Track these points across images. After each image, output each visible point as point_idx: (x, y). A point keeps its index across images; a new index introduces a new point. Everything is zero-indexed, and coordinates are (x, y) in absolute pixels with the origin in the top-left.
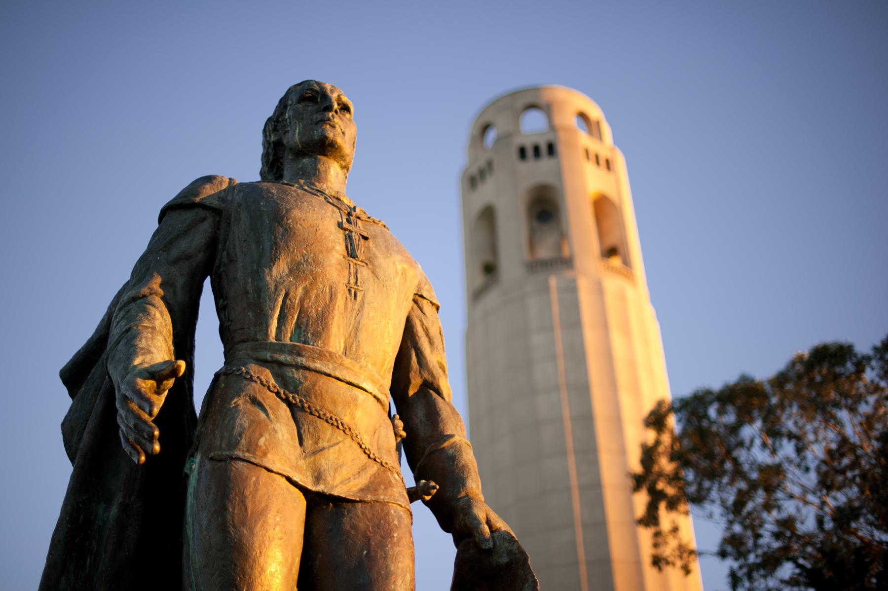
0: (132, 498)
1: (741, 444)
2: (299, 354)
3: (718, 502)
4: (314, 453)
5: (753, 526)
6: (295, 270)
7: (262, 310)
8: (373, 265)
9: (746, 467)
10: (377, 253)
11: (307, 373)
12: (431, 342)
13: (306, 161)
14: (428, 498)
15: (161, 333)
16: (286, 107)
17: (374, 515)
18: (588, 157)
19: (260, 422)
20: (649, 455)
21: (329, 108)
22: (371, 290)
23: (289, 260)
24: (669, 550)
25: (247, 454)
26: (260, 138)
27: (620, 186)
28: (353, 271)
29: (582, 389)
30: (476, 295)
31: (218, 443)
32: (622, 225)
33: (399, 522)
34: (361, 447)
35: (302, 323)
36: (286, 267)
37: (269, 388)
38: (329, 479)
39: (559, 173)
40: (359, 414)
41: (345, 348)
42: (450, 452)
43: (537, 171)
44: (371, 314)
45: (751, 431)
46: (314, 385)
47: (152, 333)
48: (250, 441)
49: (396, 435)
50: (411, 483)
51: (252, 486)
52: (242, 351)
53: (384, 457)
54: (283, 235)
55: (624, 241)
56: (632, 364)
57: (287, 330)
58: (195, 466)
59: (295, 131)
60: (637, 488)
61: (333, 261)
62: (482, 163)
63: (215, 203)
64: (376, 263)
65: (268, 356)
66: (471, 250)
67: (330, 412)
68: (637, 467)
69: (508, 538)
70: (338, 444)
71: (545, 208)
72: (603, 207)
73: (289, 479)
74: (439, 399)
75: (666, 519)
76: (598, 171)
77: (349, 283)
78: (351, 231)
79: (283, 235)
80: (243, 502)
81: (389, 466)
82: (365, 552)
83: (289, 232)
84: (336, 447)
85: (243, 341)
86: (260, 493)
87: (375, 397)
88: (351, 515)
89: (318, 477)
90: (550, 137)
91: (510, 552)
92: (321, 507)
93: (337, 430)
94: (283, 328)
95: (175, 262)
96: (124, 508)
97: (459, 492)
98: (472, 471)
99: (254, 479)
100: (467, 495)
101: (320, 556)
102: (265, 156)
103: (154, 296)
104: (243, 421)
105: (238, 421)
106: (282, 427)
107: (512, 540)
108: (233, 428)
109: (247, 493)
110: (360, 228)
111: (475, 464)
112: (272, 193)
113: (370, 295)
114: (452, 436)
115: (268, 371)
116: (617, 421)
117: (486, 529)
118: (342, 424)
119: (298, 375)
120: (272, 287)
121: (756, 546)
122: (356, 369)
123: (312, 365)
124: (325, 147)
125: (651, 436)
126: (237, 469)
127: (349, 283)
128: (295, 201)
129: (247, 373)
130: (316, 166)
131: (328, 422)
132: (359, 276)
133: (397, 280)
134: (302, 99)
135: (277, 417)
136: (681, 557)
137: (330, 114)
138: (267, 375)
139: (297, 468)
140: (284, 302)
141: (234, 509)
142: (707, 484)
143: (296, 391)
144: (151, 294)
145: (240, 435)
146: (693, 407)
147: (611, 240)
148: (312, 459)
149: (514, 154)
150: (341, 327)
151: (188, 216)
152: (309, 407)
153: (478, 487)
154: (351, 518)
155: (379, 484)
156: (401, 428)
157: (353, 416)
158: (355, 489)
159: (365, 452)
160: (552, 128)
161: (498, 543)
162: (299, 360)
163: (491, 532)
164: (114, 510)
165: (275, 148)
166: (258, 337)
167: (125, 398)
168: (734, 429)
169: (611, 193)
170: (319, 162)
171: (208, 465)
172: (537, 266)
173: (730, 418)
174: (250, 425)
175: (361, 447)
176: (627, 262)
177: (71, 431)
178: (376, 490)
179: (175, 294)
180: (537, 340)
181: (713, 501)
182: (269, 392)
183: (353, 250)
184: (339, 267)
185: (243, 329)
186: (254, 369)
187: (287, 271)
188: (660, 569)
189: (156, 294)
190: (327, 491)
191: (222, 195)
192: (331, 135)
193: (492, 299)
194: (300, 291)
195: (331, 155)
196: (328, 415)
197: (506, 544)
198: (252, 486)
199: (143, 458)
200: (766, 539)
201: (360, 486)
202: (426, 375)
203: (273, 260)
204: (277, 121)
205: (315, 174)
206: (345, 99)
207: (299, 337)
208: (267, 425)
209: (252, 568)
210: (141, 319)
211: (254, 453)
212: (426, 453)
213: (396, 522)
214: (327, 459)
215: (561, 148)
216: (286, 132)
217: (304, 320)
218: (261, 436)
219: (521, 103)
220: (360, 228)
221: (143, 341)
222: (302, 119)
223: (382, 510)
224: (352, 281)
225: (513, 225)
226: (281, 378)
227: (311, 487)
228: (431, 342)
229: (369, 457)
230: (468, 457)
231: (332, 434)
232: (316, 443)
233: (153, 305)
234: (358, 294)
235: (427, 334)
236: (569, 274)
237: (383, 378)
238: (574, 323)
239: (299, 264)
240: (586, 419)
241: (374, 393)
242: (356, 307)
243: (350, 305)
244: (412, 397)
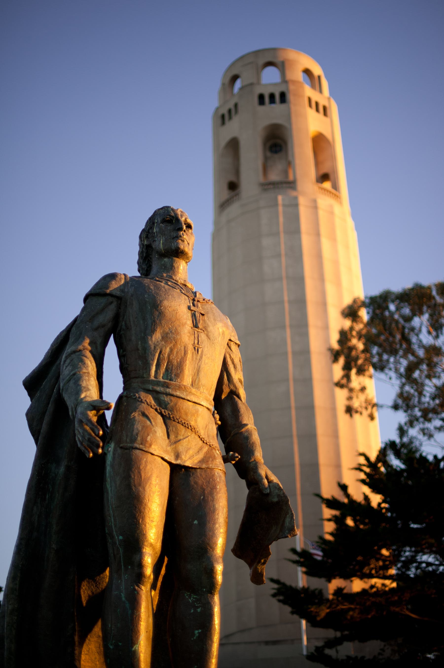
0: (72, 463)
1: (412, 329)
2: (168, 387)
3: (393, 370)
4: (176, 442)
5: (419, 387)
6: (165, 337)
7: (147, 361)
8: (207, 331)
9: (415, 347)
10: (209, 324)
11: (172, 398)
12: (235, 367)
13: (166, 260)
14: (234, 462)
15: (92, 376)
16: (154, 223)
17: (206, 476)
19: (147, 427)
20: (344, 337)
21: (181, 229)
22: (206, 347)
23: (162, 331)
24: (356, 404)
25: (141, 446)
26: (137, 241)
27: (332, 127)
28: (196, 336)
29: (299, 281)
30: (222, 206)
31: (125, 439)
32: (333, 158)
33: (220, 480)
34: (199, 437)
35: (169, 368)
36: (160, 335)
37: (151, 407)
38: (183, 457)
39: (289, 117)
40: (199, 419)
41: (192, 382)
42: (246, 434)
43: (272, 113)
44: (206, 361)
45: (421, 322)
46: (176, 405)
47: (88, 376)
48: (142, 438)
49: (216, 423)
51: (144, 463)
52: (135, 384)
53: (211, 441)
54: (158, 316)
55: (335, 170)
56: (336, 263)
57: (160, 372)
59: (160, 242)
60: (336, 356)
61: (186, 331)
62: (231, 105)
63: (118, 293)
64: (209, 330)
65: (150, 387)
66: (219, 171)
67: (184, 420)
68: (336, 346)
69: (278, 487)
70: (188, 437)
71: (277, 142)
72: (320, 142)
73: (163, 459)
74: (239, 401)
75: (356, 381)
76: (316, 118)
77: (194, 344)
78: (195, 311)
79: (158, 316)
80: (139, 473)
81: (214, 446)
82: (202, 497)
83: (161, 314)
84: (187, 439)
85: (136, 378)
86: (148, 467)
87: (207, 408)
88: (194, 476)
89: (177, 456)
90: (282, 88)
91: (279, 496)
92: (178, 472)
93: (188, 429)
94: (158, 371)
95: (96, 329)
96: (68, 468)
97: (251, 459)
98: (258, 446)
99: (145, 459)
100: (255, 460)
101: (178, 498)
103: (86, 350)
104: (138, 426)
105: (135, 427)
106: (159, 430)
107: (280, 488)
108: (133, 430)
109: (141, 467)
110: (200, 308)
111: (259, 441)
112: (151, 289)
113: (206, 350)
114: (246, 425)
115: (150, 396)
116: (324, 304)
117: (266, 481)
118: (191, 426)
119: (167, 399)
120: (152, 347)
121: (419, 402)
122: (198, 394)
123: (175, 393)
124: (179, 253)
125: (347, 323)
126: (136, 454)
127: (194, 344)
128: (165, 295)
129: (139, 397)
130: (172, 264)
131: (183, 425)
132: (200, 339)
133: (220, 339)
134: (164, 221)
135: (156, 423)
136: (366, 408)
137: (181, 233)
138: (150, 399)
139: (166, 452)
140: (159, 356)
141: (135, 476)
142: (385, 357)
143: (166, 408)
144: (84, 349)
145: (137, 435)
146: (378, 303)
147: (325, 169)
148: (174, 446)
149: (256, 100)
150: (190, 370)
151: (103, 301)
152: (173, 417)
153: (260, 456)
154: (194, 478)
155: (209, 458)
156: (218, 419)
157: (196, 421)
158: (196, 461)
159: (201, 440)
160: (285, 81)
161: (272, 490)
162: (168, 390)
163: (268, 482)
164: (62, 469)
165: (147, 249)
166: (145, 376)
167: (81, 422)
168: (408, 319)
169: (327, 133)
170: (174, 261)
171: (119, 451)
172: (269, 186)
173: (407, 311)
174: (142, 429)
175: (199, 437)
176: (335, 187)
177: (34, 420)
178: (208, 461)
179: (96, 348)
180: (266, 242)
181: (390, 369)
182: (151, 409)
183: (196, 323)
184: (189, 334)
185: (136, 370)
186: (143, 395)
187: (160, 338)
188: (351, 416)
189: (87, 349)
190: (182, 463)
191: (122, 288)
192: (182, 247)
193: (234, 209)
194: (168, 349)
195: (181, 257)
196: (183, 422)
197: (277, 491)
198: (144, 463)
199: (91, 455)
200: (426, 399)
201: (199, 459)
202: (232, 387)
203: (153, 331)
204: (148, 232)
205: (172, 269)
206: (189, 221)
207: (167, 376)
208: (151, 429)
209: (144, 509)
210: (80, 368)
211: (145, 445)
212: (232, 434)
213: (218, 480)
214: (182, 446)
215: (291, 97)
216: (154, 241)
217: (170, 367)
218: (148, 435)
219: (262, 61)
220: (200, 308)
221: (84, 382)
222: (165, 234)
223: (211, 473)
224: (196, 342)
226: (157, 400)
227: (174, 462)
228: (235, 367)
229: (203, 442)
230: (256, 438)
231: (185, 432)
232: (177, 437)
233: (86, 357)
234: (200, 350)
235: (233, 363)
236: (294, 193)
237: (210, 395)
238: (294, 230)
239: (167, 333)
240: (300, 302)
241: (207, 406)
242: (198, 358)
243: (195, 356)
244: (225, 403)
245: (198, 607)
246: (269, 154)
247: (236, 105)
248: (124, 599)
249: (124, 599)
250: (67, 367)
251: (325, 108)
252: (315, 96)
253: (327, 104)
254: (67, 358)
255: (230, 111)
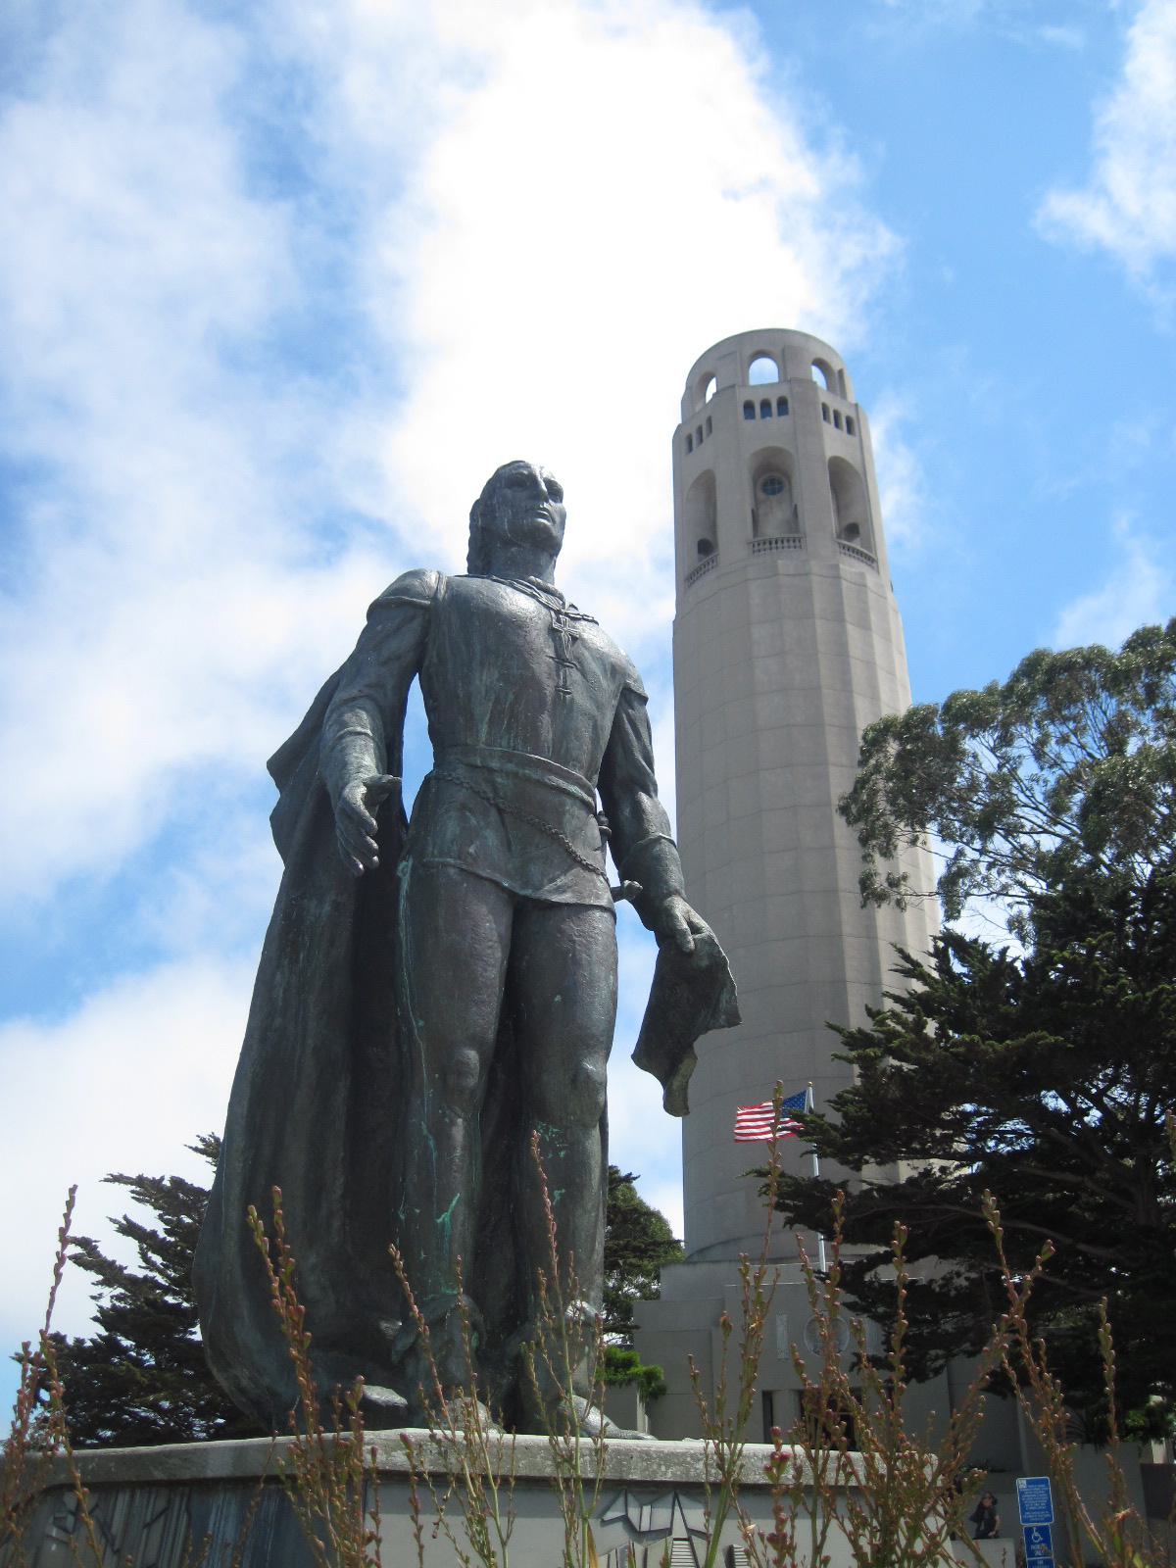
18: (826, 417)
30: (688, 579)
43: (771, 431)
50: (615, 882)
56: (870, 665)
58: (405, 868)
71: (772, 478)
90: (784, 391)
95: (385, 663)
96: (336, 906)
102: (472, 542)
149: (741, 409)
166: (468, 741)
172: (761, 544)
177: (282, 825)
193: (708, 582)
219: (749, 351)
225: (736, 499)
245: (561, 1150)
246: (761, 495)
247: (709, 421)
248: (425, 1132)
249: (425, 1132)
250: (331, 726)
251: (849, 421)
252: (834, 403)
253: (853, 415)
254: (332, 711)
255: (700, 430)
